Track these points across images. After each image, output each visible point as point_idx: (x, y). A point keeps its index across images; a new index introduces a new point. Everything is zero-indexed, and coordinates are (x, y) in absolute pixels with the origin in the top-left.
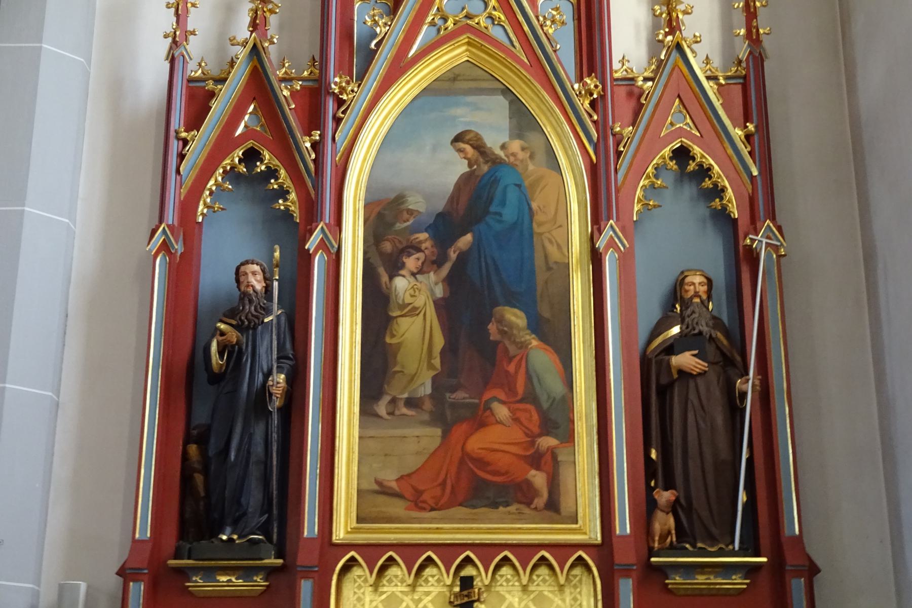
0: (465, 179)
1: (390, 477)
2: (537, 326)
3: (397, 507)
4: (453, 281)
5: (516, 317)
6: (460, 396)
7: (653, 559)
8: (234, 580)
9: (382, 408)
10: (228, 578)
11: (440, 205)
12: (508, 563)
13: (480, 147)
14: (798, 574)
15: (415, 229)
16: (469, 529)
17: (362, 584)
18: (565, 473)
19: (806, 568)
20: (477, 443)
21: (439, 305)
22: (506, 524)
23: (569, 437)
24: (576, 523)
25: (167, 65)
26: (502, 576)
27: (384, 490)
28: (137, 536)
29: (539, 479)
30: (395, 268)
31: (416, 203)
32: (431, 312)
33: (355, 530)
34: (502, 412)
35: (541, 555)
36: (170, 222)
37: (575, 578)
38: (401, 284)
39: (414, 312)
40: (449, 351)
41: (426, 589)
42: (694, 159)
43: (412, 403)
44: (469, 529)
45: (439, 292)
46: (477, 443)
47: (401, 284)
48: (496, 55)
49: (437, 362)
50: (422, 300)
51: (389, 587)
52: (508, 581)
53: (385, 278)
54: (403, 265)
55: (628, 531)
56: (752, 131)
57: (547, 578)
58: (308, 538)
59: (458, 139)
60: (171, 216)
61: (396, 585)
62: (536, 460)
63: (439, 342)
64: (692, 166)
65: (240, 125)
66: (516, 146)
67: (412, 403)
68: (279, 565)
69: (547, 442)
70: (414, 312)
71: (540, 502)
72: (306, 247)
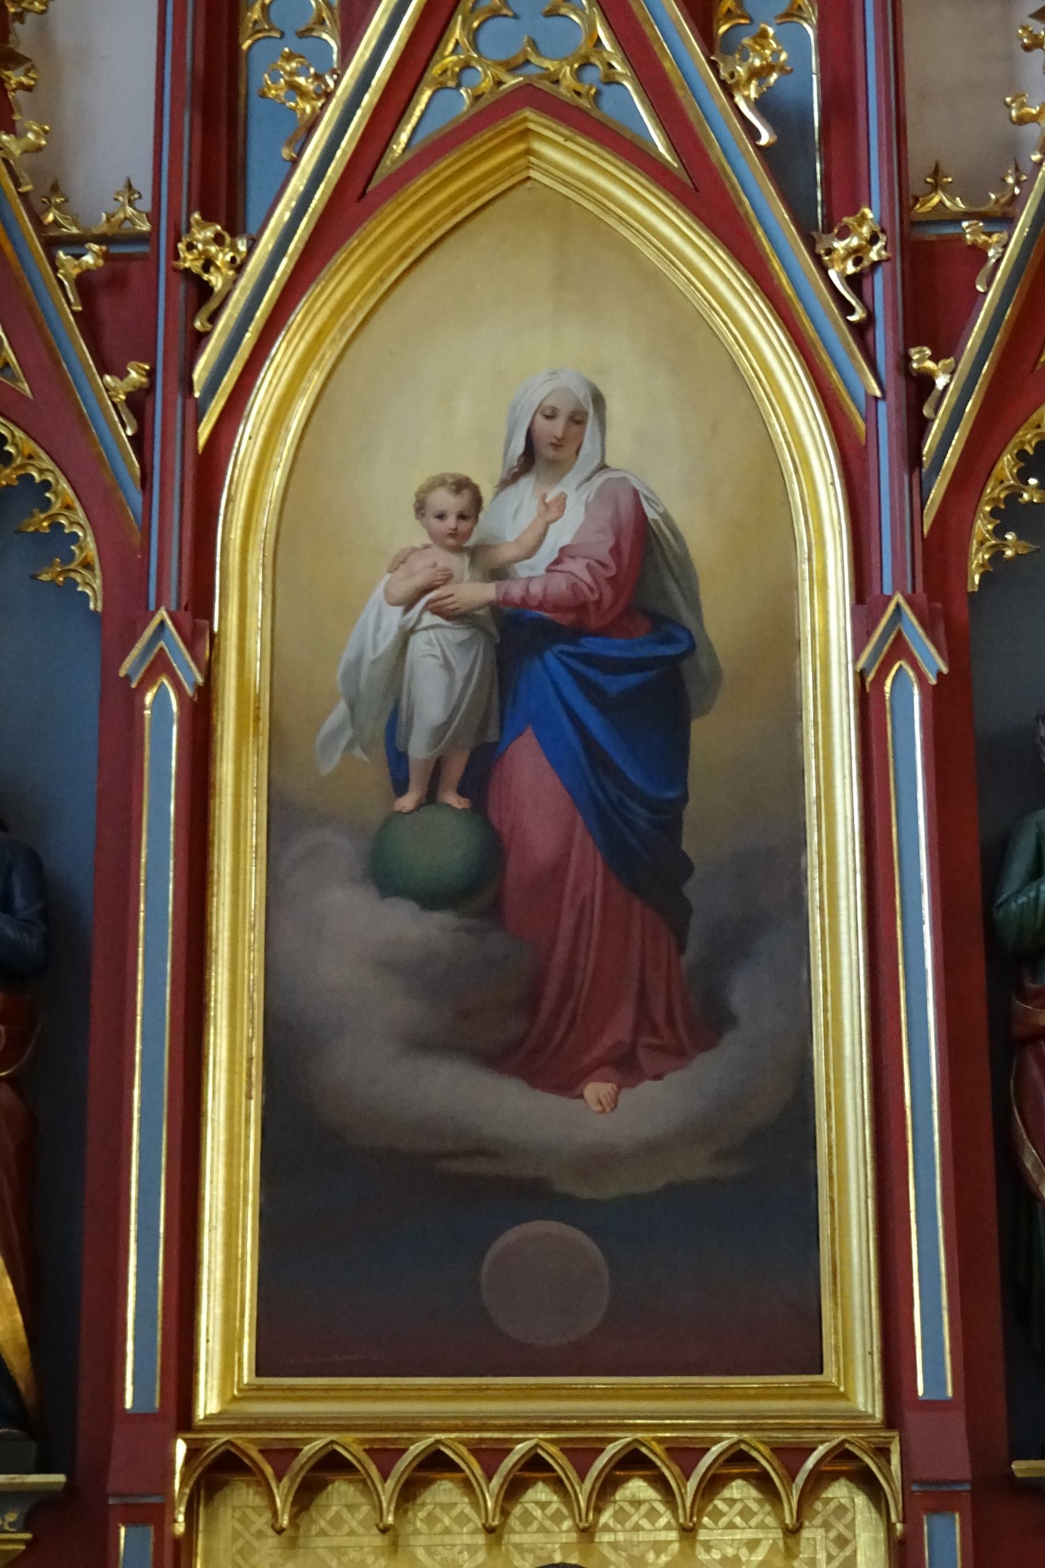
12: (449, 1475)
16: (417, 1390)
17: (738, 1520)
19: (967, 1487)
22: (323, 1375)
24: (820, 1371)
26: (731, 1502)
33: (250, 1393)
35: (738, 1449)
37: (637, 1509)
41: (335, 1542)
44: (417, 1390)
48: (333, 172)
51: (525, 1535)
52: (746, 1514)
55: (950, 1392)
56: (142, 383)
57: (754, 1506)
58: (926, 1401)
61: (731, 1526)
65: (247, 301)
68: (60, 1488)
72: (122, 673)
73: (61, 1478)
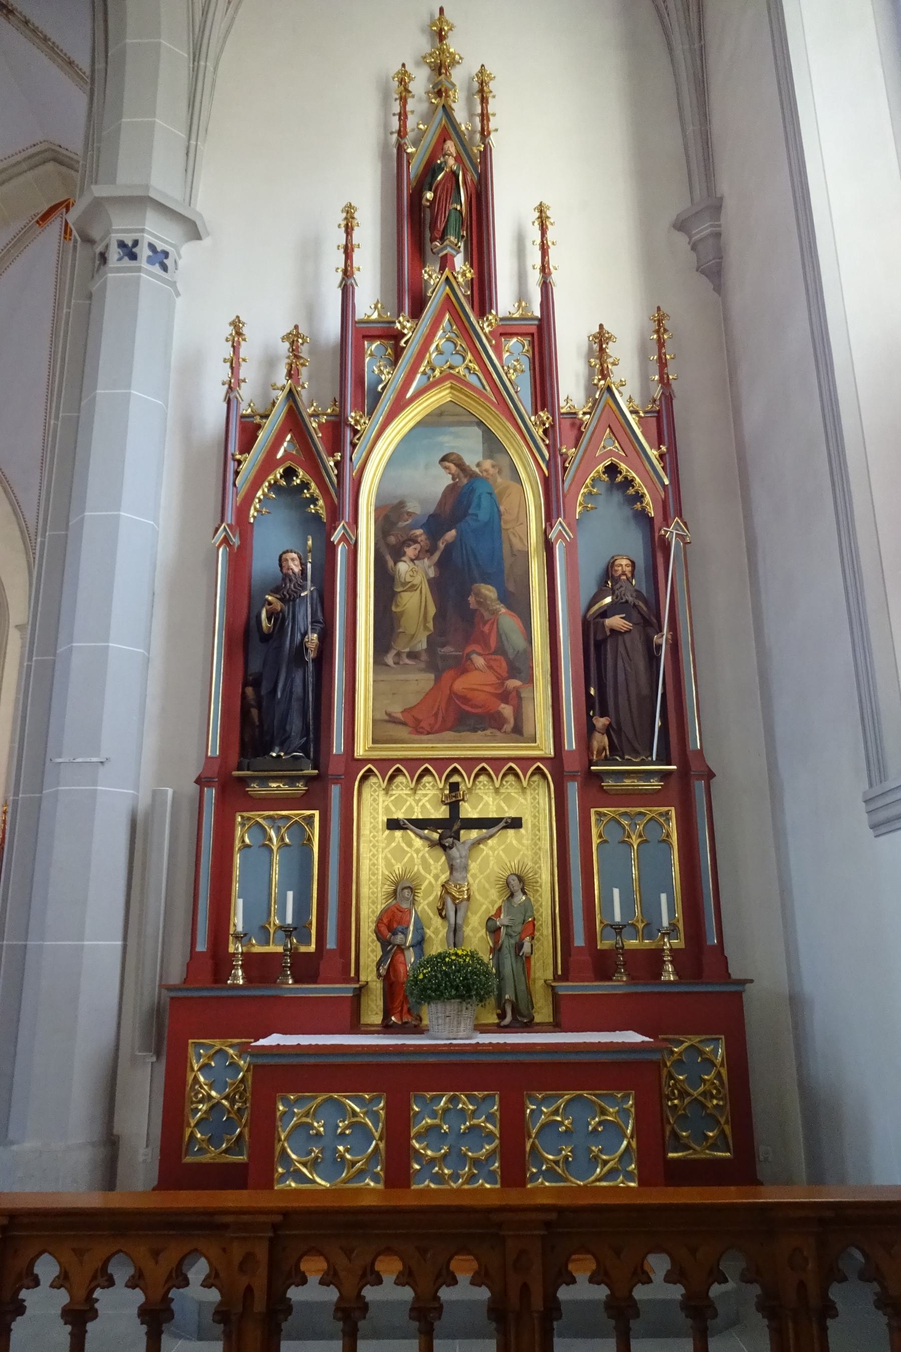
0: (450, 489)
1: (397, 710)
2: (505, 598)
3: (402, 732)
4: (441, 565)
5: (489, 592)
6: (448, 650)
7: (592, 768)
8: (281, 786)
9: (390, 659)
10: (278, 784)
11: (432, 509)
13: (461, 465)
14: (699, 777)
15: (413, 527)
18: (526, 708)
20: (461, 685)
21: (434, 584)
23: (529, 679)
25: (225, 405)
27: (392, 720)
28: (209, 754)
29: (507, 710)
30: (398, 555)
31: (413, 507)
32: (425, 588)
34: (479, 661)
36: (229, 522)
38: (403, 567)
39: (413, 588)
40: (440, 617)
42: (621, 473)
43: (413, 655)
45: (432, 573)
46: (461, 685)
47: (403, 567)
49: (431, 625)
50: (419, 579)
53: (391, 563)
54: (404, 554)
55: (574, 748)
59: (444, 459)
60: (230, 517)
62: (505, 697)
63: (432, 610)
64: (619, 478)
66: (487, 464)
67: (413, 655)
69: (513, 683)
70: (413, 588)
71: (509, 727)
72: (332, 540)
73: (316, 771)
